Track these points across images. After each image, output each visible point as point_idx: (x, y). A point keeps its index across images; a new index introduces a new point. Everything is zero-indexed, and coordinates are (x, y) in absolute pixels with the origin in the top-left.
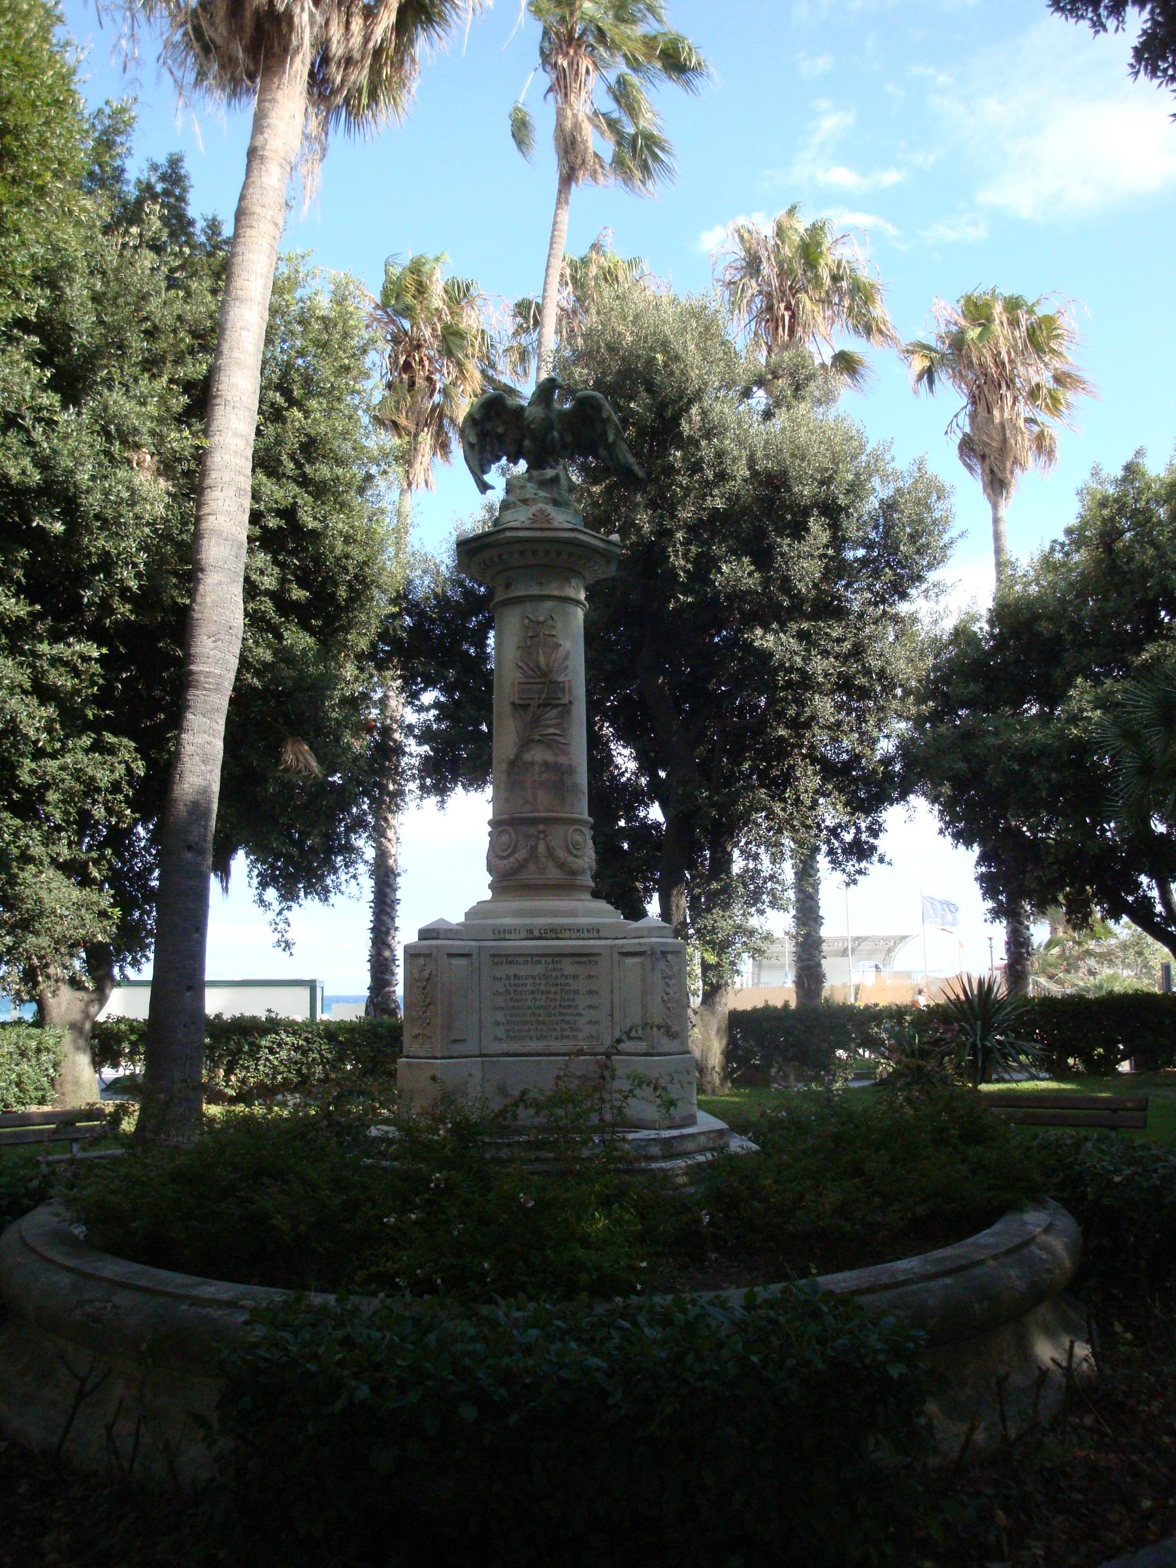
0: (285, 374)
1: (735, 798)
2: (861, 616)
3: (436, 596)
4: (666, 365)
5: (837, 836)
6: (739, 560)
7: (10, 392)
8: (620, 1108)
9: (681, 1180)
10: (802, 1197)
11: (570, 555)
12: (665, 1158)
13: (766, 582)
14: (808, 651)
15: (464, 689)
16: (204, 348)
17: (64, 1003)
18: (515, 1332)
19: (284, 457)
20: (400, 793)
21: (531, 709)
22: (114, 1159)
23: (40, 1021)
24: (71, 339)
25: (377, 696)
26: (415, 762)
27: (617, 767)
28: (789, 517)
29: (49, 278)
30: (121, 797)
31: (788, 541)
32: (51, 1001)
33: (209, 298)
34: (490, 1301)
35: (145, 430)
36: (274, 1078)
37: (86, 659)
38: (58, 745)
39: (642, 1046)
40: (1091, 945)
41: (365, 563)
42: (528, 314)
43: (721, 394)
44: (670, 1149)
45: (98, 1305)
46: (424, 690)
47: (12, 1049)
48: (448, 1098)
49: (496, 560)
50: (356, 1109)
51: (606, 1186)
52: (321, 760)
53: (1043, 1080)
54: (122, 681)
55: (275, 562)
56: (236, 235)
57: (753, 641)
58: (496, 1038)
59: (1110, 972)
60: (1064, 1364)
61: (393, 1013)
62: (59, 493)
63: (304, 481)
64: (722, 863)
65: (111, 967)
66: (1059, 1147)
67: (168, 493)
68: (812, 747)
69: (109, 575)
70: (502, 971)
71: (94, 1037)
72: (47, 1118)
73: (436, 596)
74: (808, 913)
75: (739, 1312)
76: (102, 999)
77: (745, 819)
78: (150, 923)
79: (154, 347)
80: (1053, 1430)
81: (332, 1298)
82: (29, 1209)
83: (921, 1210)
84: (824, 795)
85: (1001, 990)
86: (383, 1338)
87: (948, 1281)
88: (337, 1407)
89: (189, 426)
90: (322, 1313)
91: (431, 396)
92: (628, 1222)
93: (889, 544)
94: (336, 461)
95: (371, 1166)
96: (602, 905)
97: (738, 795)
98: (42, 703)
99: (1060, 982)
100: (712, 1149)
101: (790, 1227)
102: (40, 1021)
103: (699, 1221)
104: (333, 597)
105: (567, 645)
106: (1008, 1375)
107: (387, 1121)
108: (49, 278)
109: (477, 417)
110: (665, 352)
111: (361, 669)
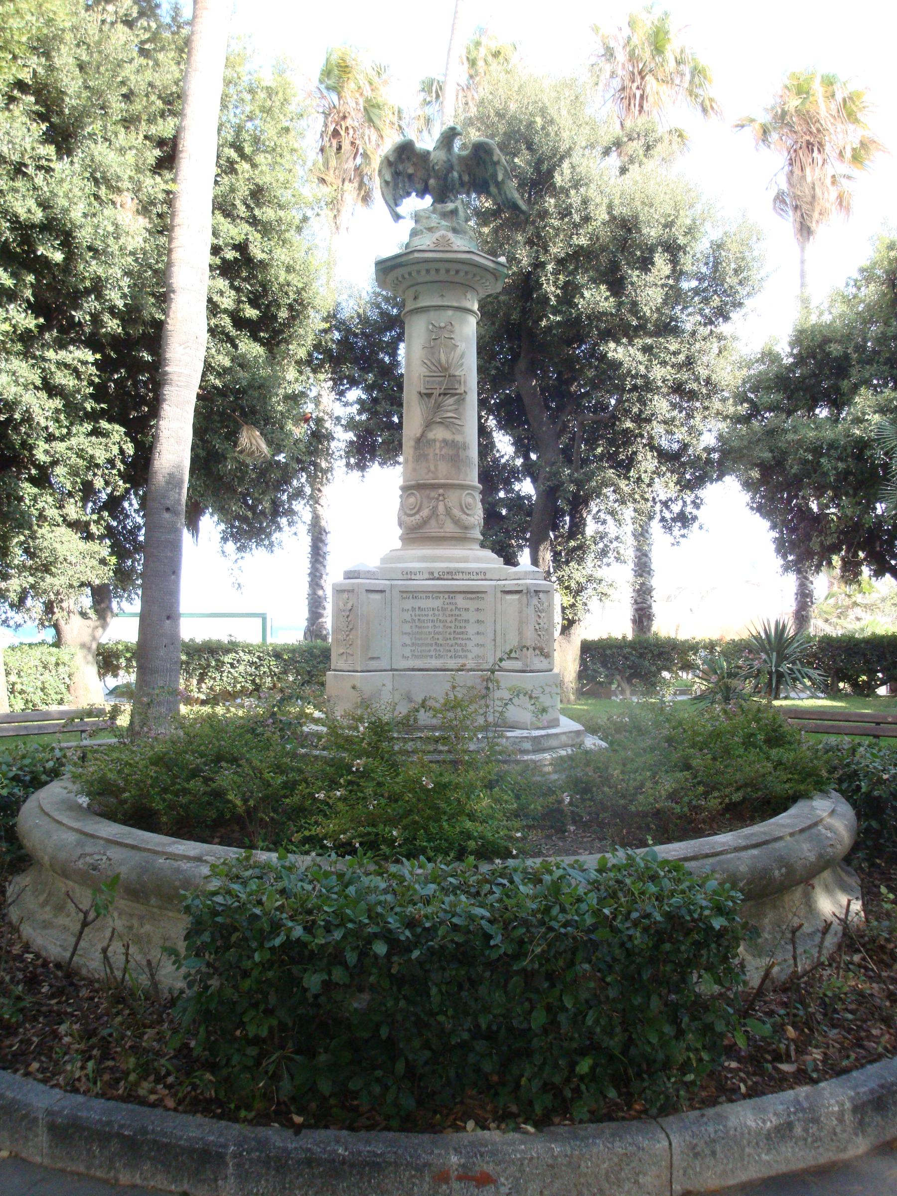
0: (238, 133)
1: (590, 477)
2: (694, 333)
3: (359, 316)
4: (543, 128)
5: (668, 507)
6: (598, 288)
7: (14, 144)
8: (501, 713)
9: (549, 769)
10: (642, 785)
11: (466, 273)
12: (535, 751)
13: (620, 304)
14: (650, 361)
15: (381, 389)
16: (174, 114)
17: (77, 630)
18: (417, 886)
19: (238, 202)
20: (329, 470)
21: (434, 397)
22: (112, 748)
23: (57, 644)
24: (63, 100)
25: (312, 394)
26: (343, 445)
27: (498, 451)
28: (638, 253)
29: (43, 47)
30: (115, 472)
31: (637, 273)
32: (65, 628)
33: (174, 67)
34: (397, 861)
35: (126, 177)
36: (235, 686)
37: (84, 363)
38: (65, 431)
39: (518, 665)
40: (859, 598)
41: (303, 289)
42: (433, 90)
43: (587, 152)
44: (538, 745)
45: (97, 857)
46: (349, 389)
47: (37, 663)
48: (365, 704)
49: (406, 276)
50: (294, 710)
51: (489, 773)
52: (269, 443)
53: (819, 698)
54: (115, 381)
55: (232, 287)
56: (195, 17)
57: (607, 353)
58: (403, 656)
59: (872, 618)
60: (843, 916)
61: (324, 638)
62: (57, 228)
63: (254, 222)
64: (577, 527)
65: (110, 602)
66: (839, 750)
67: (147, 230)
68: (651, 438)
69: (99, 297)
70: (409, 604)
71: (98, 655)
72: (61, 715)
73: (359, 316)
74: (643, 567)
75: (593, 875)
76: (104, 626)
77: (597, 493)
78: (140, 568)
79: (131, 108)
80: (830, 965)
81: (274, 856)
82: (46, 783)
83: (737, 797)
84: (659, 475)
85: (790, 631)
86: (314, 889)
87: (755, 852)
88: (277, 942)
89: (160, 175)
90: (266, 867)
91: (354, 158)
92: (506, 802)
93: (716, 275)
94: (279, 206)
95: (306, 755)
96: (488, 554)
97: (593, 474)
98: (50, 396)
99: (835, 625)
100: (573, 746)
101: (633, 809)
102: (57, 644)
103: (561, 802)
104: (275, 317)
105: (462, 346)
106: (801, 926)
107: (316, 721)
108: (43, 47)
109: (392, 159)
110: (543, 117)
111: (301, 373)
